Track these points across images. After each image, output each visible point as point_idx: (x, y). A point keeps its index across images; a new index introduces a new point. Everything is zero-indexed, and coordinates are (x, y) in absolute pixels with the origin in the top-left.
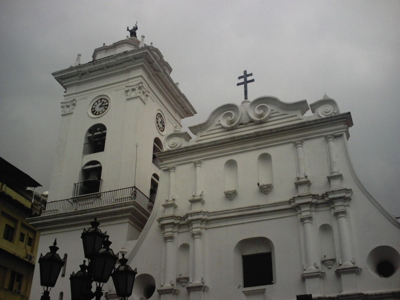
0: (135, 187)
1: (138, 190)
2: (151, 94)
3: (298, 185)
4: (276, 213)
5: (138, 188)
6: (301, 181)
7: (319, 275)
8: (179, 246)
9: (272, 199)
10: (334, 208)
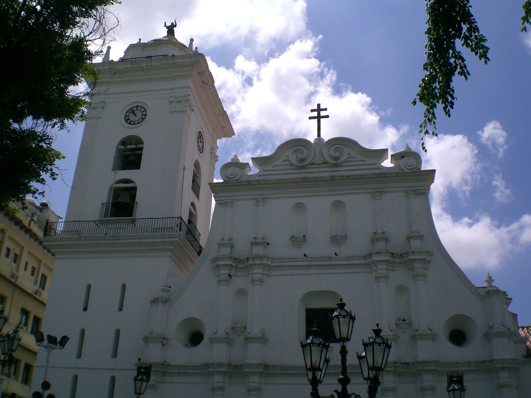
0: (181, 218)
3: (374, 240)
6: (378, 236)
9: (344, 250)
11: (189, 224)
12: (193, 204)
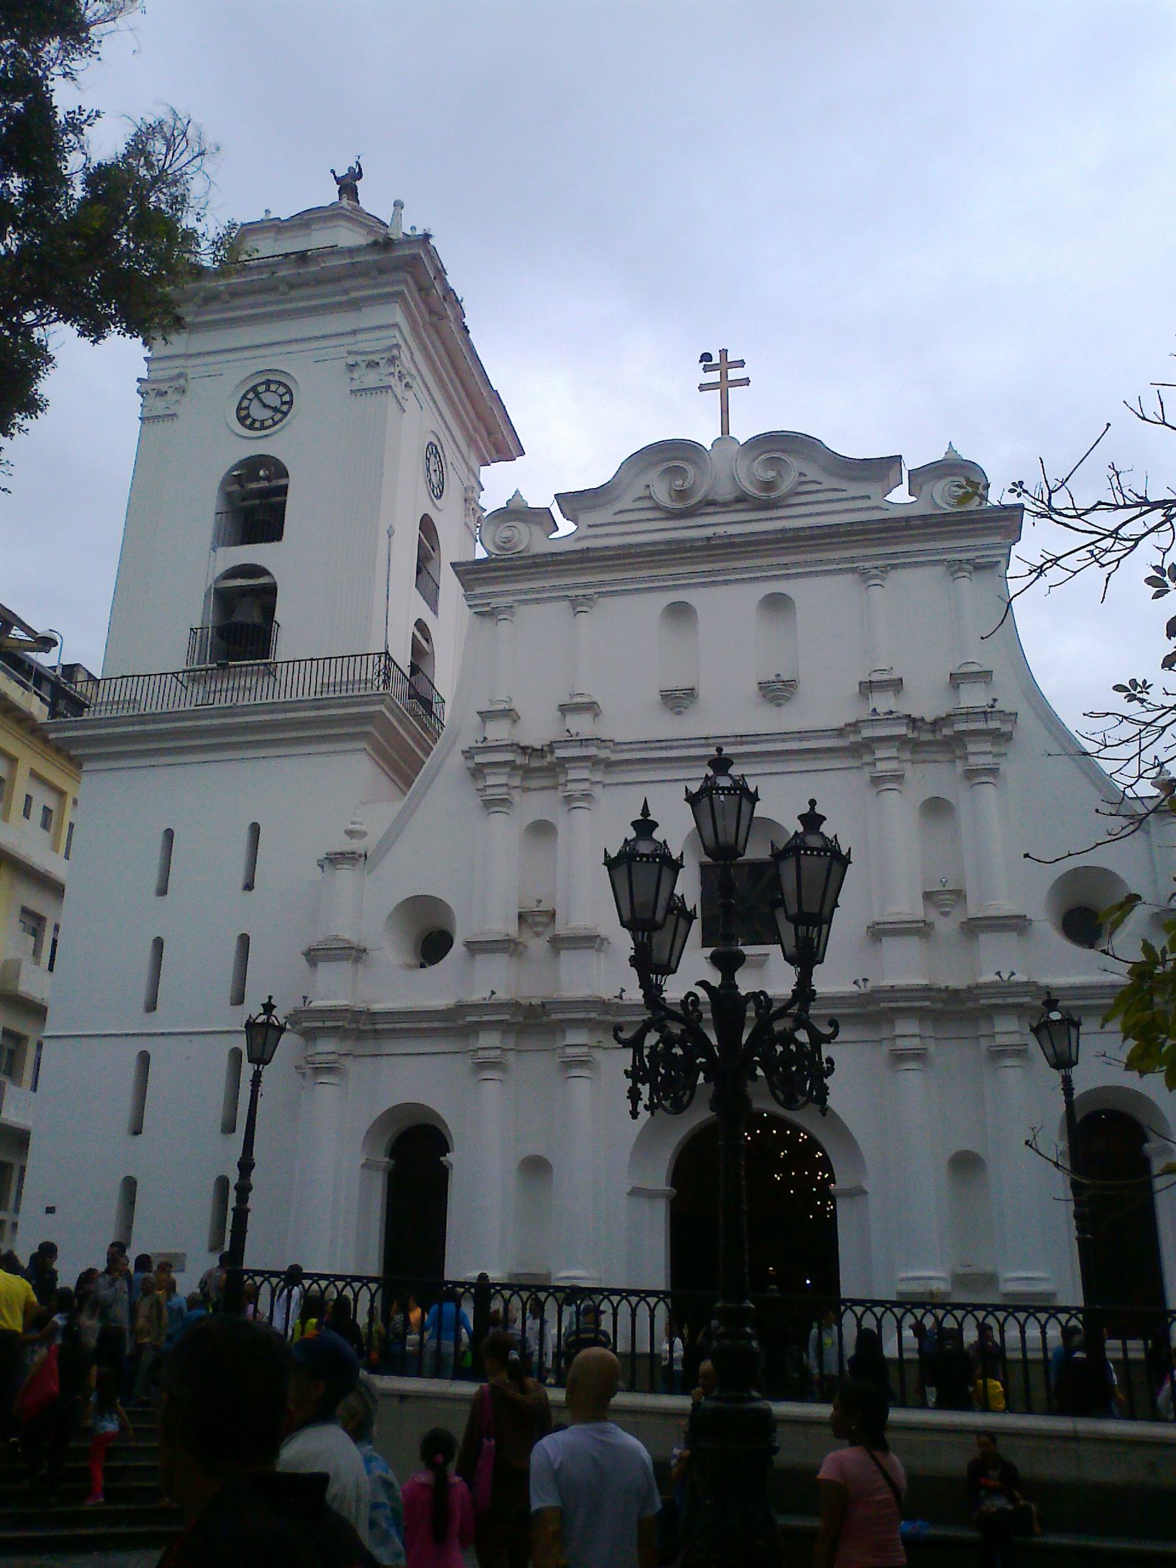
1: (395, 663)
2: (417, 385)
4: (643, 766)
5: (394, 659)
7: (921, 927)
8: (524, 827)
10: (965, 757)
11: (413, 678)
12: (420, 625)
